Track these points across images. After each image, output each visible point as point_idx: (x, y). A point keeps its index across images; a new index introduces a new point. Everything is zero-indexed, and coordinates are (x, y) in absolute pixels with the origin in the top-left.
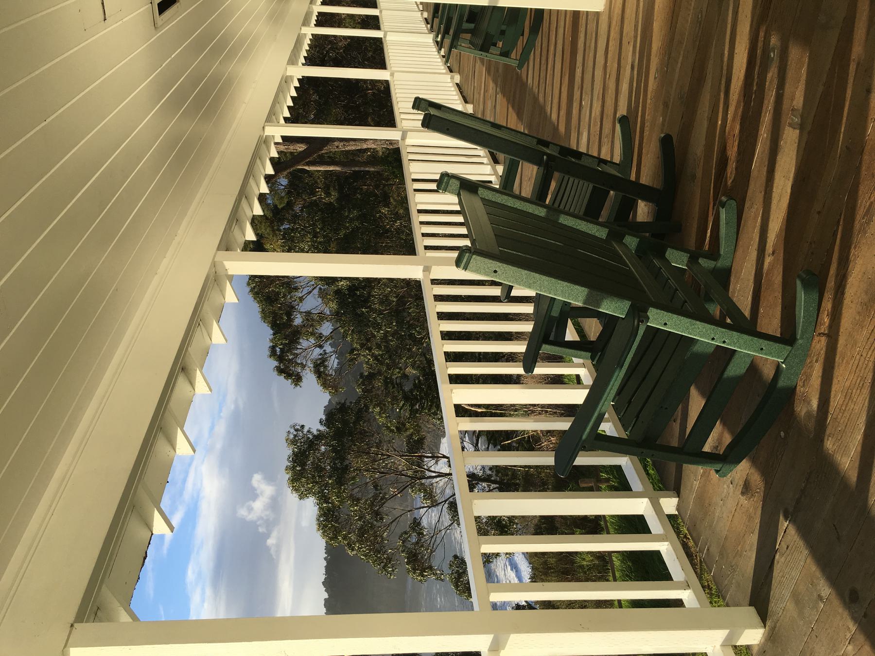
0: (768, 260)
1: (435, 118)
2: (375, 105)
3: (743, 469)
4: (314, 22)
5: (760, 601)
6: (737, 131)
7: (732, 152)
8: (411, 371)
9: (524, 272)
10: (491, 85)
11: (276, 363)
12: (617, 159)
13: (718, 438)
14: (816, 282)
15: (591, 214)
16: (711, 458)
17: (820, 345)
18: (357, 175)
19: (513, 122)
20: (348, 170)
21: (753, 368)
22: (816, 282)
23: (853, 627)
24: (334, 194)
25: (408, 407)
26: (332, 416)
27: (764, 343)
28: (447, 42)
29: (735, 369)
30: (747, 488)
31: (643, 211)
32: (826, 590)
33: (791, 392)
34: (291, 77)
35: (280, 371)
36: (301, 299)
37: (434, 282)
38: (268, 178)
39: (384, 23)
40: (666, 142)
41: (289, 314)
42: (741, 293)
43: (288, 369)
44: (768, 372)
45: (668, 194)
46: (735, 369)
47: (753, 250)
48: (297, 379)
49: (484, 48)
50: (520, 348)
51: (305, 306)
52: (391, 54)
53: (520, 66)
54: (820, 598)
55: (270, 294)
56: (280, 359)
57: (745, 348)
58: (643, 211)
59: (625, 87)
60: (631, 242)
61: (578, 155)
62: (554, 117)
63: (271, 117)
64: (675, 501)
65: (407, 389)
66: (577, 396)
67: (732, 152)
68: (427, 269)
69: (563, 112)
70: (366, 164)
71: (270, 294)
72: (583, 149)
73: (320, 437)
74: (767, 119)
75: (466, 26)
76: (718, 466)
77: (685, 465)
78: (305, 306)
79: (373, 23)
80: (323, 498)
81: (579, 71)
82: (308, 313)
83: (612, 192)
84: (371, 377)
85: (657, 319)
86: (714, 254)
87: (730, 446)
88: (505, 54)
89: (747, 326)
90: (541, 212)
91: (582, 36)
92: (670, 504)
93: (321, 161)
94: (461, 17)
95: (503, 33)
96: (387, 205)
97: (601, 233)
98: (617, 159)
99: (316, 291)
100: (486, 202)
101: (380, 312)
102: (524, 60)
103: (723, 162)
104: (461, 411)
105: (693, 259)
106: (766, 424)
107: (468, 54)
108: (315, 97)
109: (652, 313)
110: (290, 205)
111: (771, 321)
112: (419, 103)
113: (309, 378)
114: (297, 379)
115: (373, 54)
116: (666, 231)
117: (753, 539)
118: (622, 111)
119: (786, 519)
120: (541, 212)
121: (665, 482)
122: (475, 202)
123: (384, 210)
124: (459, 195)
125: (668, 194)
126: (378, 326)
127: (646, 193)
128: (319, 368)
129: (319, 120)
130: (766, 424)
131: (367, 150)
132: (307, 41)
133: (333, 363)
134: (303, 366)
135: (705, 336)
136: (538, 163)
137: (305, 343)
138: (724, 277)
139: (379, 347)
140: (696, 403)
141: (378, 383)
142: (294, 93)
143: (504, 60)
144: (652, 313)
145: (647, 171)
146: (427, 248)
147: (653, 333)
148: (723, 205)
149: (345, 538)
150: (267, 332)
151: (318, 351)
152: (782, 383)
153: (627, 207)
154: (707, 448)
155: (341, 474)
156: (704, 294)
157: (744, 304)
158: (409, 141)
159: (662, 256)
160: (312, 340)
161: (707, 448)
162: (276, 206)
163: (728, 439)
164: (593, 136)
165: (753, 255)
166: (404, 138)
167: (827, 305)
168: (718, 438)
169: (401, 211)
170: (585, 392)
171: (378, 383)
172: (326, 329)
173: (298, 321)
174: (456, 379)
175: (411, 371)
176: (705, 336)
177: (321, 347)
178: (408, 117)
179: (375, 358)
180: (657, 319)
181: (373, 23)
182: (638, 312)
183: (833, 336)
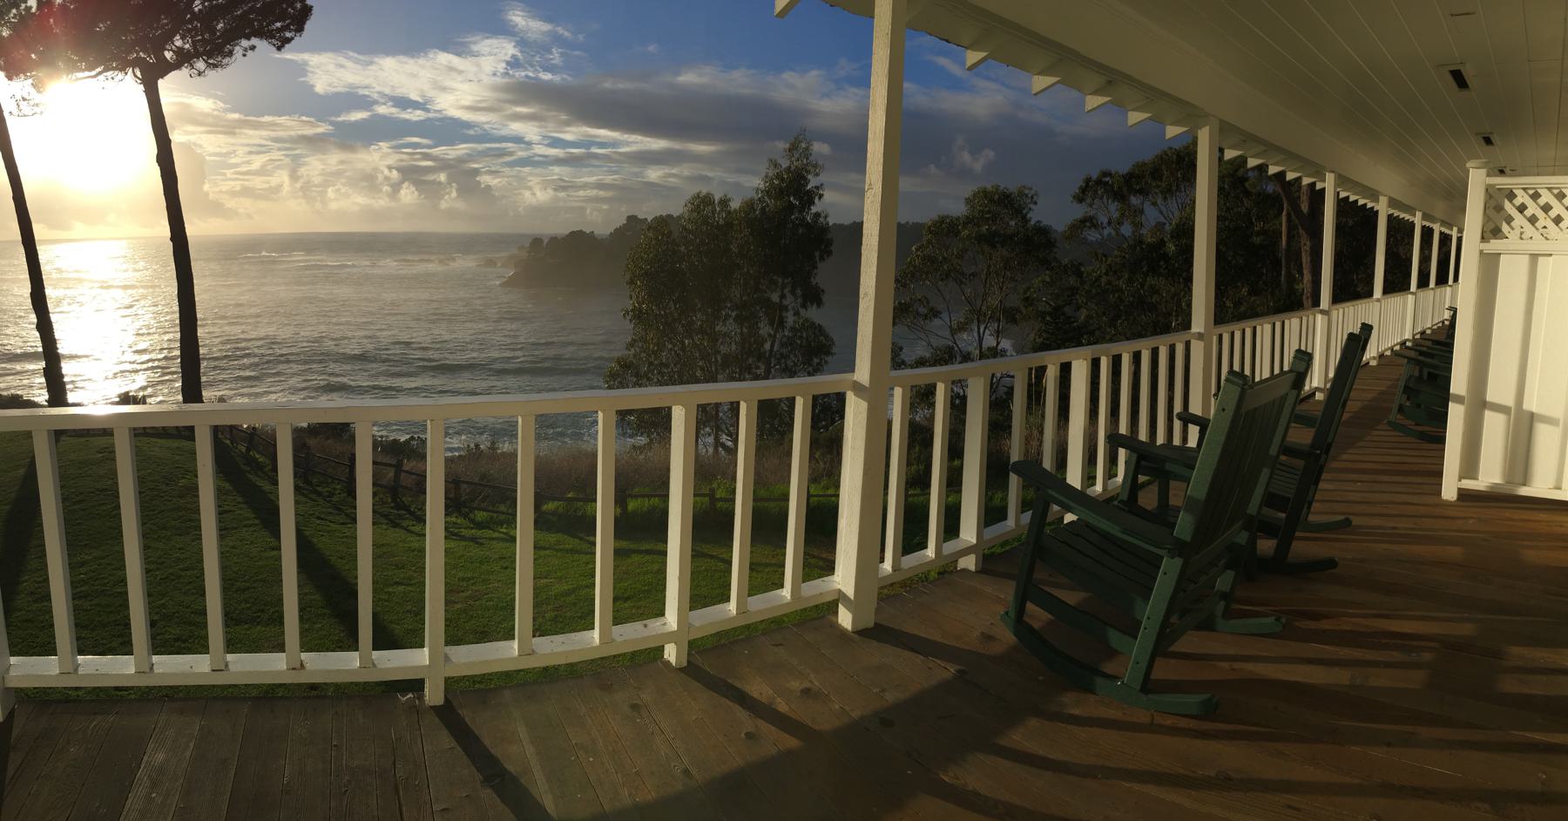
0: (1226, 665)
1: (1357, 342)
2: (1351, 287)
3: (1007, 637)
4: (1427, 224)
5: (873, 633)
6: (1344, 627)
7: (1325, 625)
8: (1083, 315)
9: (1223, 439)
10: (1370, 396)
11: (1095, 177)
12: (1311, 518)
13: (1037, 615)
14: (1209, 711)
15: (1271, 500)
16: (1021, 610)
17: (1143, 717)
18: (1277, 263)
19: (1346, 416)
20: (1282, 255)
21: (1112, 653)
22: (1209, 711)
23: (856, 714)
24: (1257, 240)
25: (1048, 309)
26: (1043, 231)
27: (1144, 665)
28: (1412, 354)
29: (1115, 638)
30: (988, 638)
31: (1266, 546)
32: (891, 697)
33: (1089, 689)
34: (1377, 201)
35: (1088, 181)
36: (1154, 204)
37: (1188, 344)
38: (1281, 175)
39: (1422, 294)
40: (1331, 563)
41: (1141, 192)
42: (1190, 642)
43: (1088, 190)
44: (1109, 668)
45: (1279, 566)
46: (1115, 638)
47: (1239, 651)
48: (1080, 199)
49: (1407, 389)
50: (1143, 436)
51: (1148, 208)
52: (1395, 300)
53: (1389, 423)
54: (883, 690)
55: (1177, 166)
56: (1099, 182)
57: (1137, 650)
58: (1266, 546)
59: (1376, 522)
60: (1242, 538)
61: (1317, 484)
62: (1344, 457)
63: (1342, 180)
64: (972, 568)
65: (1066, 309)
66: (1074, 478)
67: (1325, 625)
68: (1200, 336)
69: (1349, 465)
70: (1289, 275)
71: (1177, 166)
72: (1322, 485)
73: (1025, 220)
74: (1357, 654)
75: (1426, 371)
76: (1012, 615)
77: (1013, 583)
78: (1148, 208)
79: (1423, 283)
80: (968, 221)
81: (1386, 478)
82: (1142, 212)
83: (1283, 515)
84: (1079, 274)
85: (1170, 567)
86: (1229, 614)
87: (1031, 629)
88: (1401, 409)
89: (1161, 648)
90: (1273, 451)
91: (1419, 480)
92: (969, 563)
93: (1290, 228)
94: (1436, 367)
95: (1419, 406)
96: (1250, 294)
97: (1252, 508)
98: (1311, 518)
99: (1162, 219)
100: (1284, 398)
101: (1142, 285)
102: (1394, 426)
103: (1315, 617)
104: (1066, 369)
105: (1225, 596)
106: (1058, 660)
107: (1403, 371)
108: (1351, 223)
109: (1178, 562)
110: (1247, 193)
111: (1165, 670)
112: (1367, 328)
113: (1080, 211)
114: (1080, 199)
115: (1396, 283)
116: (1250, 567)
117: (936, 637)
118: (1356, 521)
119: (958, 671)
120: (1273, 451)
121: (992, 560)
122: (1285, 387)
123: (1244, 291)
124: (1290, 371)
125: (1279, 566)
126: (1130, 281)
127: (1284, 547)
128: (1088, 222)
129: (1340, 229)
130: (1058, 660)
131: (1302, 274)
132: (1407, 217)
133: (1092, 236)
134: (1091, 206)
135: (1151, 612)
136: (1313, 446)
137: (1114, 207)
138: (1207, 625)
139: (1109, 283)
140: (1072, 598)
141: (1073, 281)
142: (1361, 202)
143: (1395, 408)
144: (1178, 562)
145: (1302, 548)
146: (1221, 337)
147: (1155, 563)
148: (1278, 620)
149: (929, 242)
150: (1122, 166)
151: (1105, 220)
152: (1099, 681)
153: (1269, 529)
154: (1030, 606)
155: (991, 240)
156: (1188, 608)
157: (1180, 646)
158: (1319, 317)
159: (1227, 567)
160: (1116, 215)
161: (1030, 606)
162: (1247, 179)
163: (1036, 625)
164: (1334, 495)
165: (1231, 651)
166: (1322, 312)
167: (1183, 723)
168: (1037, 615)
169: (1242, 309)
170: (1078, 485)
171: (1073, 281)
172: (1127, 230)
173: (1135, 200)
174: (1095, 364)
175: (1083, 315)
176: (1151, 612)
177: (1109, 223)
178: (1351, 316)
179: (1098, 279)
180: (1170, 567)
181: (1423, 283)
182: (1180, 549)
183: (1152, 728)
